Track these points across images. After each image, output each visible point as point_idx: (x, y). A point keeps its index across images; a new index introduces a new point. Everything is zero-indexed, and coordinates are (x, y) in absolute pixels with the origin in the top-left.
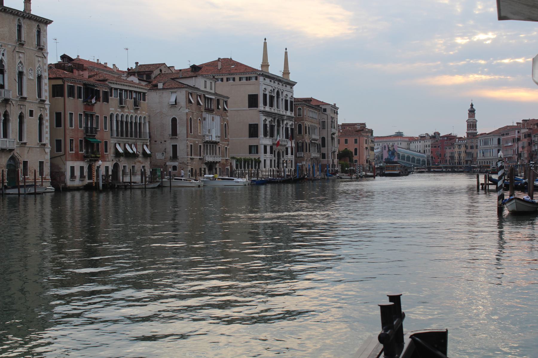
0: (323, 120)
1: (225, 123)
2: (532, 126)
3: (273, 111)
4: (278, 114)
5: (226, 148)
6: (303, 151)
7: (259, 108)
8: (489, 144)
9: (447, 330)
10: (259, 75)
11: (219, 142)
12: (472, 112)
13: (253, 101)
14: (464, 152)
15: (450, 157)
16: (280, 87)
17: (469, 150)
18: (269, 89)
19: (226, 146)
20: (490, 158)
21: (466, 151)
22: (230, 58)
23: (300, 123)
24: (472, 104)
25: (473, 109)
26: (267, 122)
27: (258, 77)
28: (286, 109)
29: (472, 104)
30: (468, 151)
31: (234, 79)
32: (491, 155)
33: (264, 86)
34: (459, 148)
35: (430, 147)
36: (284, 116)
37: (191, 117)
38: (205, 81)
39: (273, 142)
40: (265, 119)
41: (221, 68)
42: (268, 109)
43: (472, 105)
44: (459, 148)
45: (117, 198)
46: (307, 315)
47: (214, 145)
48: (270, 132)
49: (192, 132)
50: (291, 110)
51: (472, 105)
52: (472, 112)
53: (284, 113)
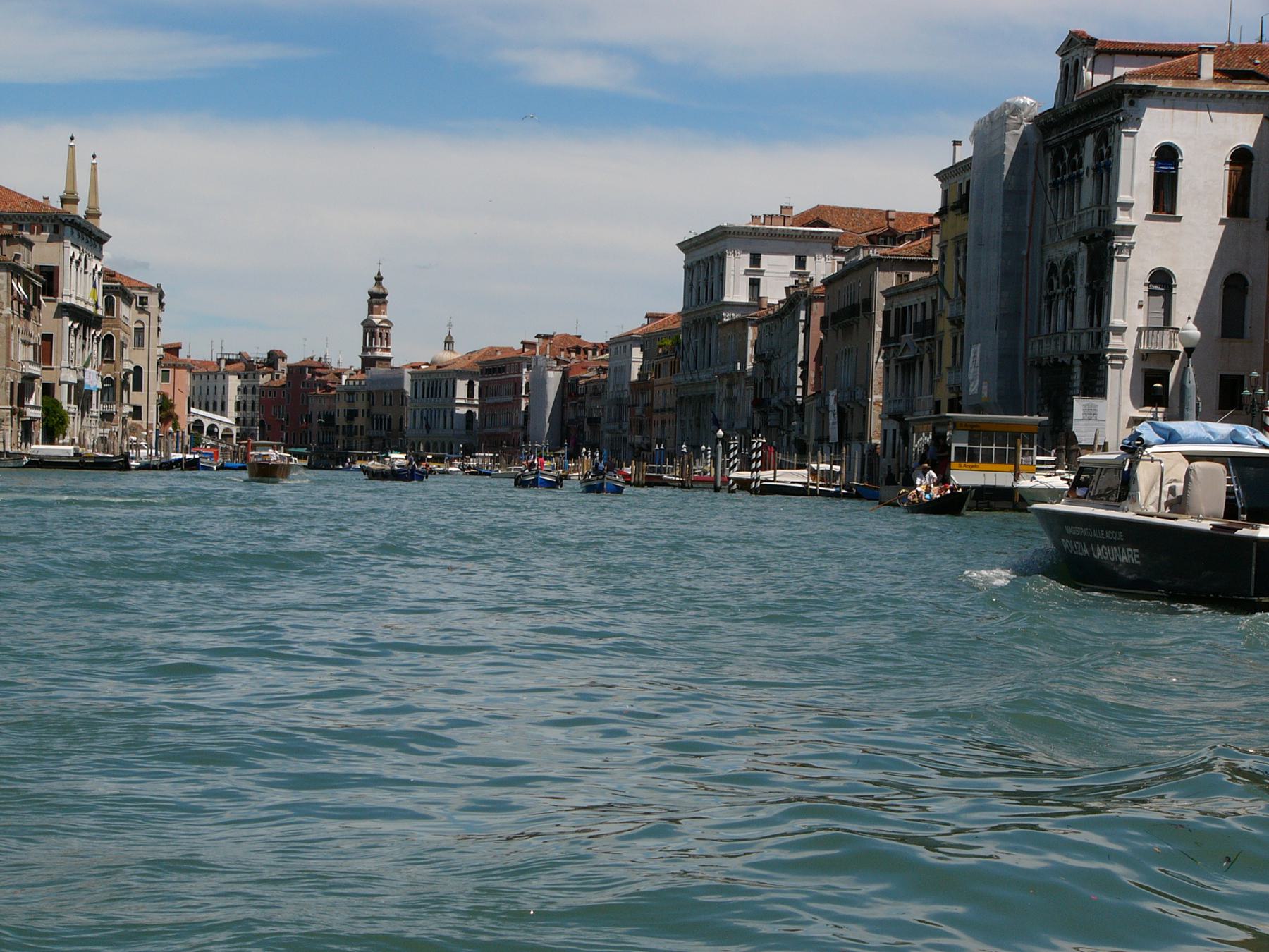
0: (140, 326)
2: (563, 353)
7: (59, 298)
9: (1179, 219)
10: (64, 222)
12: (377, 299)
14: (366, 411)
17: (378, 409)
21: (369, 411)
23: (109, 332)
24: (379, 273)
25: (381, 291)
27: (61, 226)
29: (379, 273)
30: (375, 410)
34: (351, 402)
35: (257, 395)
43: (379, 279)
44: (351, 402)
46: (359, 709)
51: (379, 279)
52: (377, 299)
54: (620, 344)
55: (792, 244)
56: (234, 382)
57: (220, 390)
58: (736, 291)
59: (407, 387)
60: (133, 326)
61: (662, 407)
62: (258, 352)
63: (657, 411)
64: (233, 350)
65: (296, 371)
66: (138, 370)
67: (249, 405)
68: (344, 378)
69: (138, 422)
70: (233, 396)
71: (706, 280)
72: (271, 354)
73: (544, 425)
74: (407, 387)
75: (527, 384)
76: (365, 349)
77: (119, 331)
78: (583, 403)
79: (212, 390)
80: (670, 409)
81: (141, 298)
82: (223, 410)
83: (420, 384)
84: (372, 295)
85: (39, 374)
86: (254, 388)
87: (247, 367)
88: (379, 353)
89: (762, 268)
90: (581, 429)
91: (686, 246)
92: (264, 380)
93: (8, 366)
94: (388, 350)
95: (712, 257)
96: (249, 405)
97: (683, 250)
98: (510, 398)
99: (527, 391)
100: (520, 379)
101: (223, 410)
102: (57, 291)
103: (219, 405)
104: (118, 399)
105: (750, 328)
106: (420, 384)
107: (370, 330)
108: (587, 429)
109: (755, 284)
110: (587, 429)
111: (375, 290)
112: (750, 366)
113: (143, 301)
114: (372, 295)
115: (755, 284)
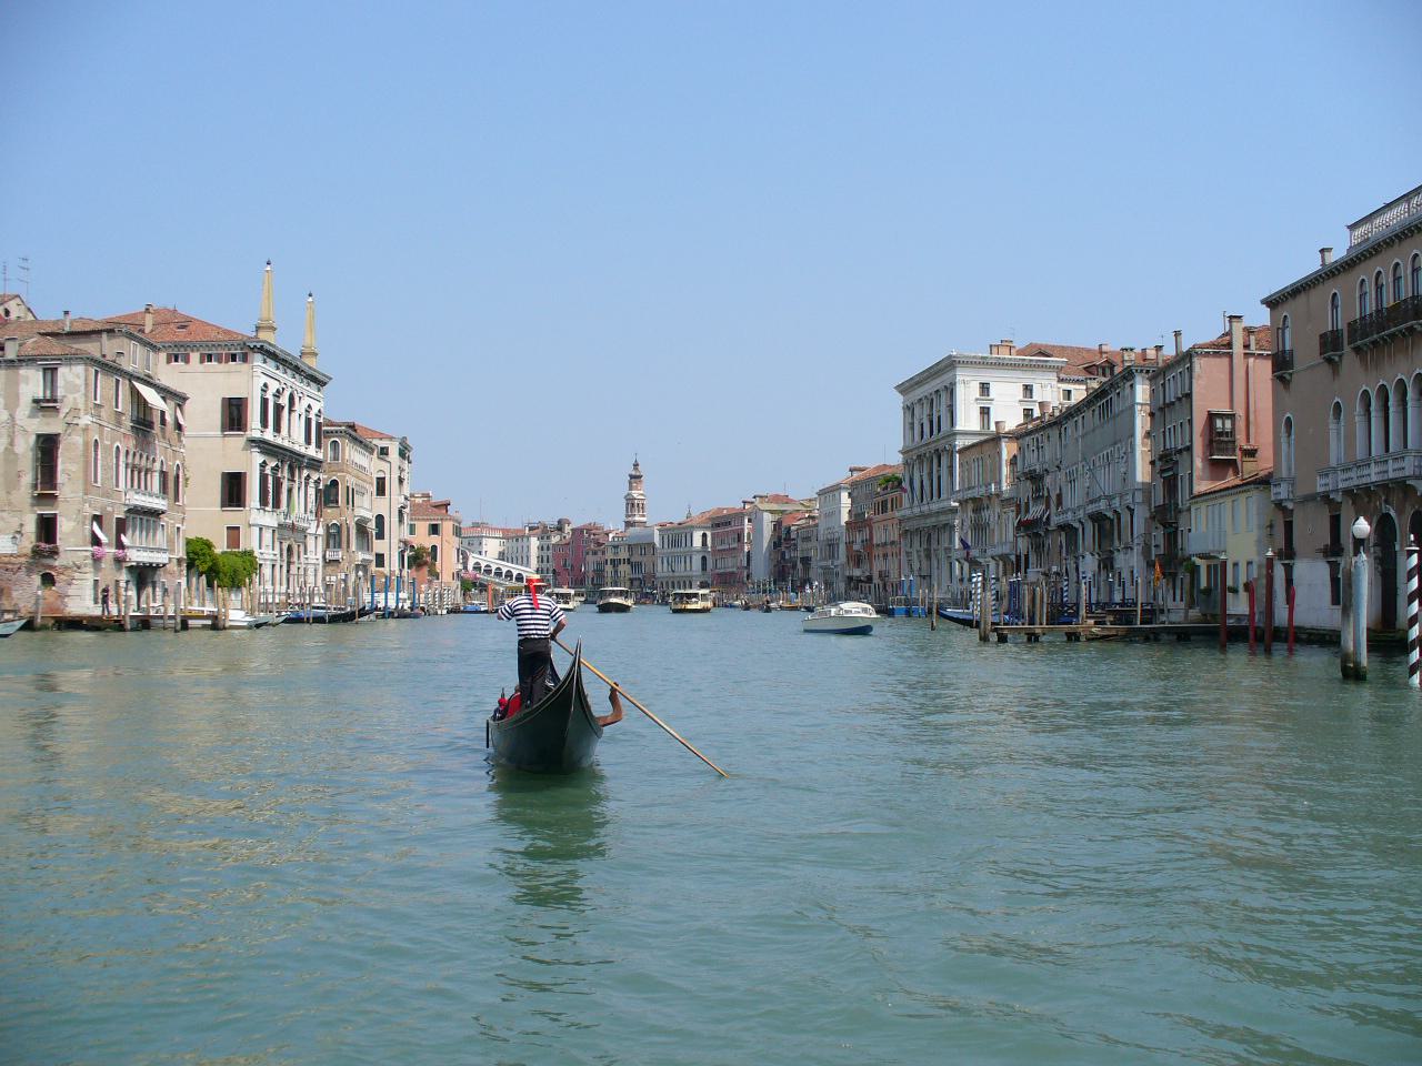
0: (381, 475)
1: (178, 462)
3: (279, 441)
4: (291, 452)
5: (178, 528)
6: (340, 546)
7: (248, 433)
8: (683, 545)
11: (163, 513)
13: (234, 415)
15: (594, 571)
16: (298, 385)
18: (273, 386)
19: (177, 525)
20: (685, 574)
22: (171, 308)
23: (334, 478)
26: (268, 471)
28: (308, 441)
31: (187, 360)
32: (688, 569)
33: (264, 379)
36: (303, 456)
37: (97, 437)
38: (118, 381)
39: (279, 519)
40: (264, 462)
41: (152, 331)
42: (269, 435)
43: (636, 465)
45: (1251, 633)
47: (152, 519)
48: (271, 496)
49: (99, 480)
50: (319, 446)
51: (636, 465)
53: (302, 450)
54: (830, 492)
55: (1019, 374)
56: (534, 542)
57: (525, 549)
58: (967, 420)
59: (657, 540)
60: (375, 476)
61: (558, 637)
62: (552, 521)
63: (878, 545)
64: (535, 520)
65: (577, 532)
66: (380, 519)
67: (545, 559)
68: (611, 536)
69: (381, 569)
70: (534, 552)
71: (931, 415)
72: (559, 522)
73: (761, 570)
74: (657, 540)
75: (749, 534)
76: (628, 516)
77: (344, 477)
78: (795, 545)
79: (520, 549)
80: (893, 543)
81: (382, 449)
82: (528, 565)
83: (666, 537)
84: (632, 477)
85: (164, 508)
86: (548, 547)
87: (544, 532)
88: (637, 518)
89: (991, 397)
90: (794, 567)
91: (904, 389)
92: (555, 539)
93: (86, 494)
94: (644, 516)
95: (938, 391)
96: (545, 559)
97: (901, 392)
98: (735, 545)
99: (749, 538)
100: (743, 530)
101: (528, 565)
102: (246, 425)
103: (525, 559)
104: (344, 545)
105: (1003, 444)
106: (666, 537)
107: (631, 504)
108: (800, 566)
109: (985, 412)
110: (800, 566)
111: (634, 473)
112: (1005, 487)
113: (384, 452)
114: (632, 477)
115: (985, 412)
